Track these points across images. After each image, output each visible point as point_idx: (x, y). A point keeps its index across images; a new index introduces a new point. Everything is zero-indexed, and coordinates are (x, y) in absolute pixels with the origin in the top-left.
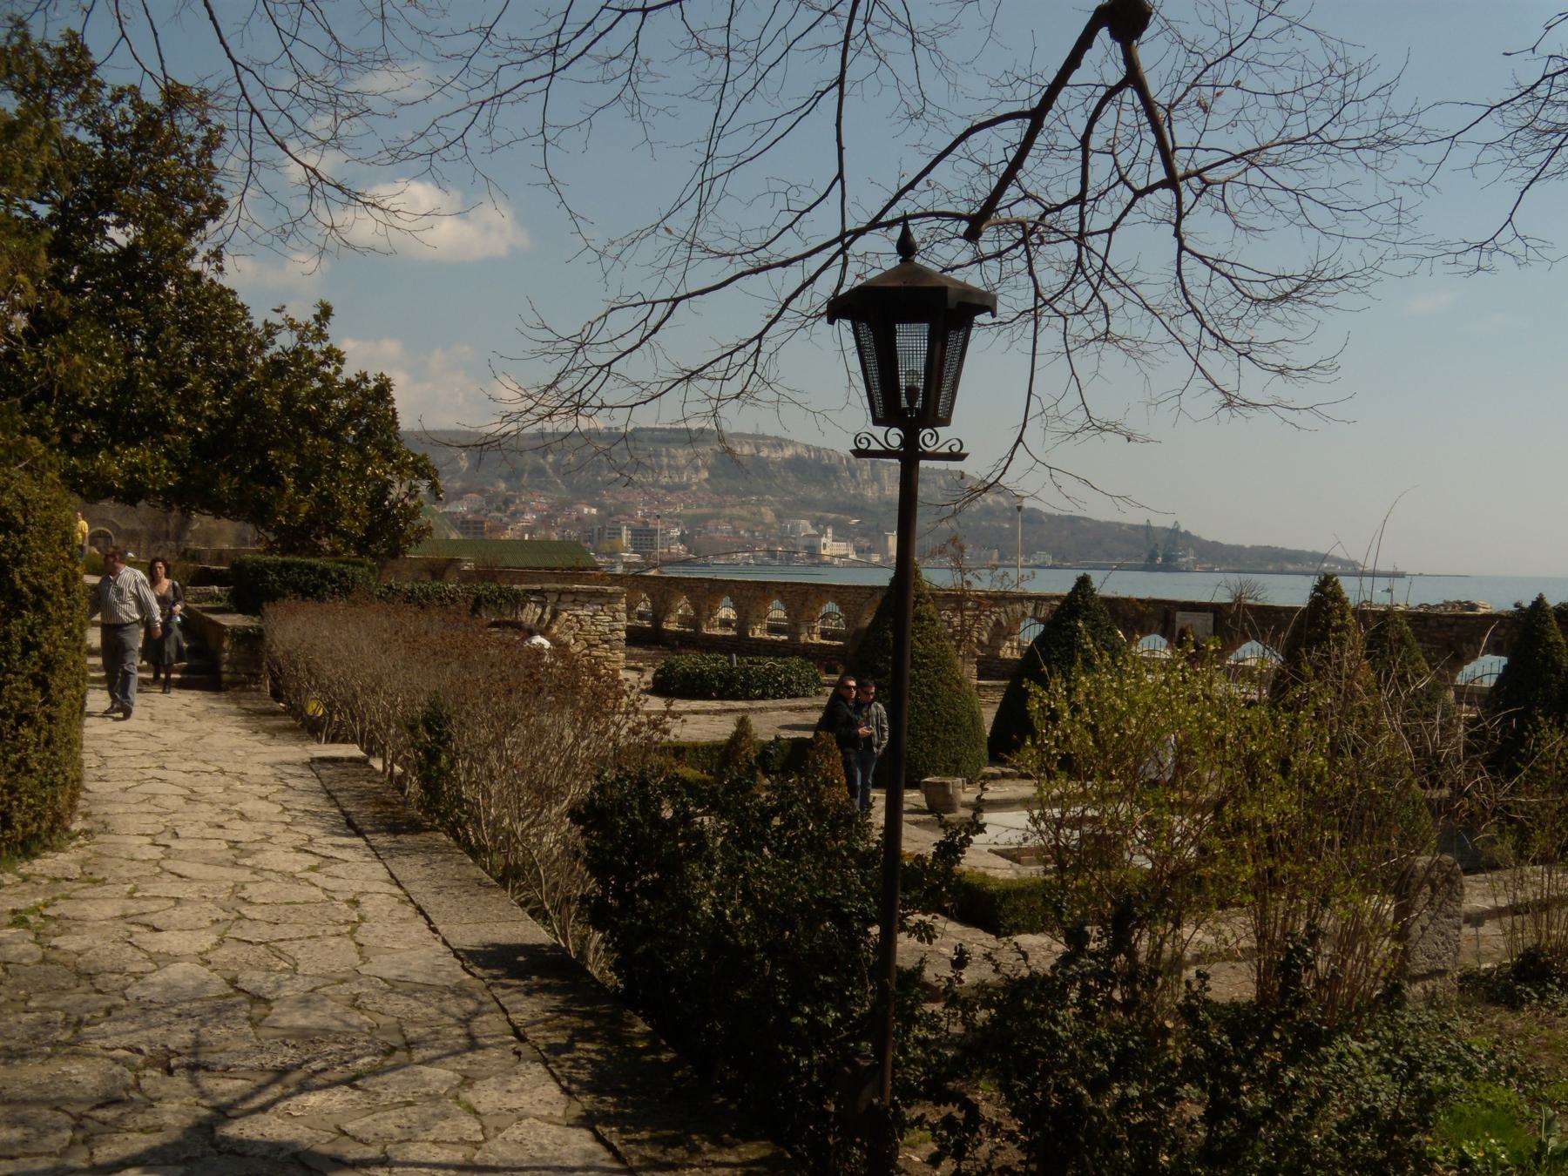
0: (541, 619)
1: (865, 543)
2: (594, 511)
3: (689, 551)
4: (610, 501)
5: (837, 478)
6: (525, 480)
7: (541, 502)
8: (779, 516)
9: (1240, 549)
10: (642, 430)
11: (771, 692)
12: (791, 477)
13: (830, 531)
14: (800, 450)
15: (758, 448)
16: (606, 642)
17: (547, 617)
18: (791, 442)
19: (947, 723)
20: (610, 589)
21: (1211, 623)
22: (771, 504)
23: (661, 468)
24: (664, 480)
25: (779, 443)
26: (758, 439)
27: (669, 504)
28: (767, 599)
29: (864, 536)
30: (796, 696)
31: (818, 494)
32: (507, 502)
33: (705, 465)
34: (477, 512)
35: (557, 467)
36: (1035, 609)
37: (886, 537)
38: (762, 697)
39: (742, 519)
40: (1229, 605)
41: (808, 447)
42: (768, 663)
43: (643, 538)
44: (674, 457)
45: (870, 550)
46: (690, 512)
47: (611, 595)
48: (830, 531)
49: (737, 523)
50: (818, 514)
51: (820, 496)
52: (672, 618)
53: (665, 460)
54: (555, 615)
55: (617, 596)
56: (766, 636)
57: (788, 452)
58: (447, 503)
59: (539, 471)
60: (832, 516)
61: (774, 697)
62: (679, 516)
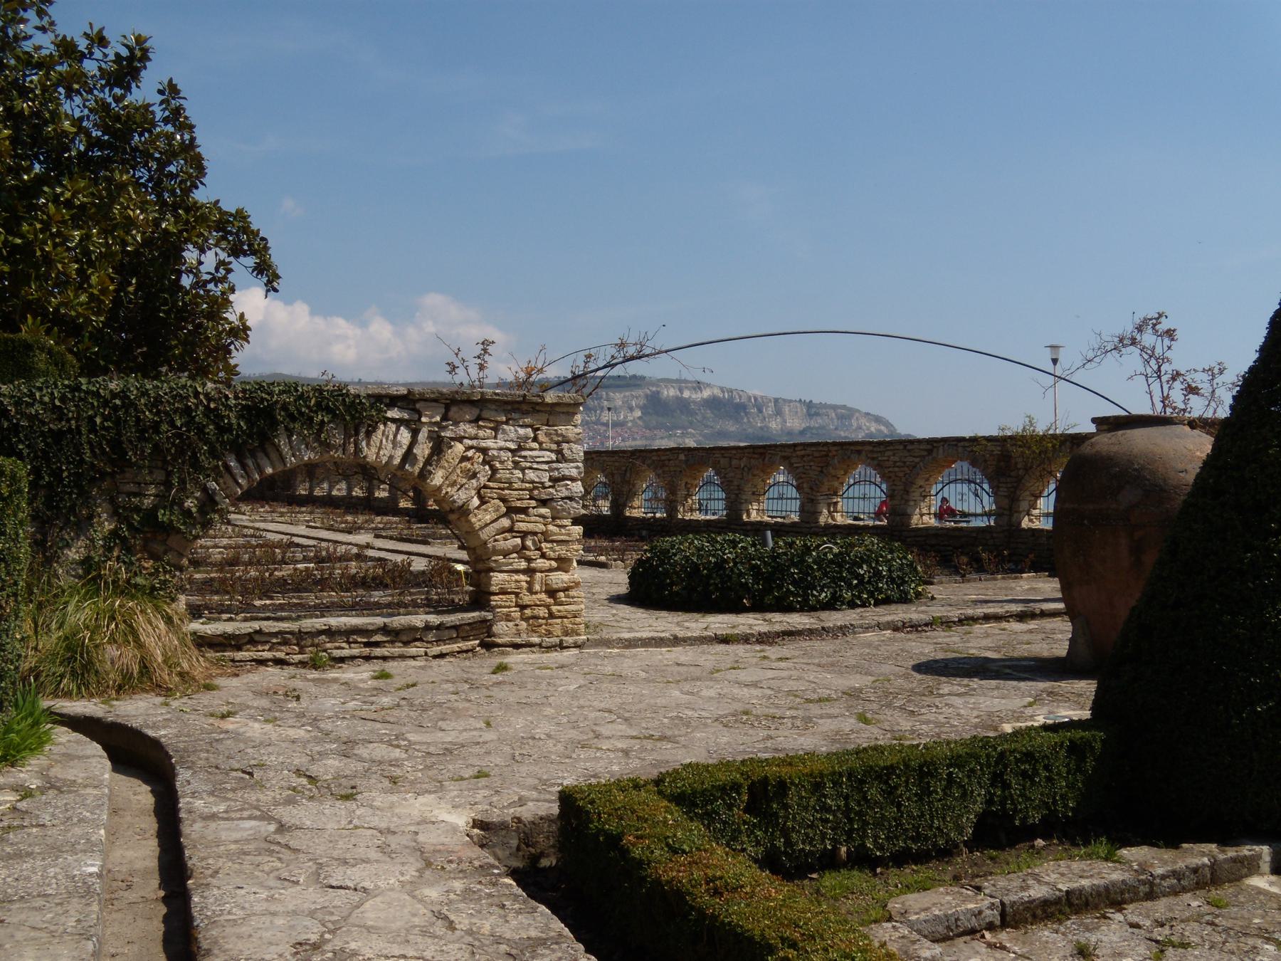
0: (409, 456)
5: (746, 414)
11: (847, 595)
12: (709, 414)
14: (717, 392)
15: (681, 390)
16: (544, 503)
17: (422, 450)
18: (708, 385)
22: (693, 436)
25: (699, 386)
26: (680, 383)
28: (768, 469)
30: (887, 601)
41: (722, 389)
51: (733, 429)
52: (636, 503)
54: (439, 446)
57: (706, 394)
61: (852, 605)
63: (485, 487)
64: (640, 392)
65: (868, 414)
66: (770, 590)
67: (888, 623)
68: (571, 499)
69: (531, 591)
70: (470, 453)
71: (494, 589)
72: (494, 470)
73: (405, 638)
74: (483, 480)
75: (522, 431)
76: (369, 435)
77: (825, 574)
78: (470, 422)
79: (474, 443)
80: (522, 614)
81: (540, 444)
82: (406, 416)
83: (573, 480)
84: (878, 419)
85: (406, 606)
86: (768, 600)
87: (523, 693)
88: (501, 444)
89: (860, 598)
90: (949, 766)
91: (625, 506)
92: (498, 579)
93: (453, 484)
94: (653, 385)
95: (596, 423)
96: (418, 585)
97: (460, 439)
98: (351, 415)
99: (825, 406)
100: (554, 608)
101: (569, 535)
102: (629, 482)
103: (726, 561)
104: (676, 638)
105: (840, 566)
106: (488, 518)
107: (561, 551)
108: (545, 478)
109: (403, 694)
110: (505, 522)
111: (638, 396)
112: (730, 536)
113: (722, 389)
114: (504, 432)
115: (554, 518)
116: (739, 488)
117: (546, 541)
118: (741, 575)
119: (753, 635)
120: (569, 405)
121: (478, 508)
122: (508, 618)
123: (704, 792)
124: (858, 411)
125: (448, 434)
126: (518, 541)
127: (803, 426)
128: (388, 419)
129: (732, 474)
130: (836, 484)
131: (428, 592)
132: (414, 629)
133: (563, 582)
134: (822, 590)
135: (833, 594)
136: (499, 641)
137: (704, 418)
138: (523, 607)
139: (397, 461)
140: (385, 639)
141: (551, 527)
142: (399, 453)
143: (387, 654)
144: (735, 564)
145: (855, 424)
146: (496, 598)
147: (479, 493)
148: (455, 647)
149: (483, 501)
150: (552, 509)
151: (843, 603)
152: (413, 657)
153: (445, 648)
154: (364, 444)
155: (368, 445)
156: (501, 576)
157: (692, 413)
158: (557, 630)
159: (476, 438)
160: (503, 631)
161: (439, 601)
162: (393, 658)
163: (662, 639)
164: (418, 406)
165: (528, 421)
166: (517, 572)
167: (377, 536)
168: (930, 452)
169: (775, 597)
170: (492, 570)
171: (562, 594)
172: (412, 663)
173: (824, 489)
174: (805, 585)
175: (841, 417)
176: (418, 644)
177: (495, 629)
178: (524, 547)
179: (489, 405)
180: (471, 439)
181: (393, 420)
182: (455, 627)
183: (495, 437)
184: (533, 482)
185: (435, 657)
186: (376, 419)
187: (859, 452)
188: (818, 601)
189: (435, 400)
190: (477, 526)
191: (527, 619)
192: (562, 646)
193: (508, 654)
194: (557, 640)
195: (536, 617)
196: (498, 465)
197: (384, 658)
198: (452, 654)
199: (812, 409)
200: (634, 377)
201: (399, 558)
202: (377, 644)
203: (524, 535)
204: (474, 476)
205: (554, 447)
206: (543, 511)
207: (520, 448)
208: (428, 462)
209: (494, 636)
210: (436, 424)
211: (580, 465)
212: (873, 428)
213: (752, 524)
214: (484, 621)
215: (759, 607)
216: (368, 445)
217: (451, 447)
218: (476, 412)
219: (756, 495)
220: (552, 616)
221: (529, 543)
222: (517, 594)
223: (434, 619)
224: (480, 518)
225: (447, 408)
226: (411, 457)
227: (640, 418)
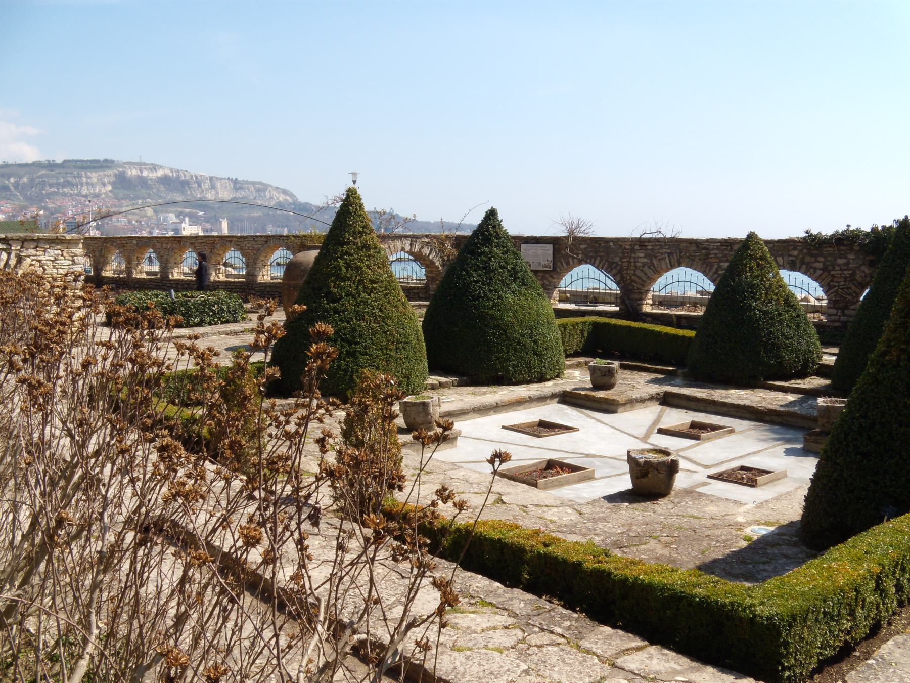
1: (208, 226)
4: (51, 206)
5: (190, 188)
8: (155, 212)
9: (428, 223)
10: (69, 161)
11: (208, 319)
12: (162, 188)
13: (187, 219)
17: (13, 262)
18: (161, 167)
19: (399, 342)
21: (551, 252)
24: (85, 191)
25: (154, 168)
28: (182, 250)
29: (207, 221)
30: (227, 322)
33: (109, 183)
35: (16, 185)
36: (411, 245)
37: (221, 222)
38: (200, 324)
40: (567, 238)
41: (171, 170)
44: (90, 178)
48: (187, 219)
50: (179, 210)
52: (108, 268)
53: (84, 180)
54: (20, 260)
57: (160, 173)
60: (187, 210)
61: (210, 324)
64: (111, 172)
65: (278, 188)
70: (34, 262)
75: (56, 252)
77: (197, 310)
84: (285, 192)
88: (47, 258)
91: (101, 270)
94: (120, 167)
95: (77, 195)
97: (29, 256)
99: (247, 182)
105: (204, 306)
111: (109, 175)
112: (155, 292)
113: (171, 170)
116: (167, 260)
124: (271, 186)
130: (219, 258)
137: (158, 191)
145: (268, 196)
157: (149, 187)
159: (36, 255)
165: (59, 247)
168: (266, 242)
173: (213, 261)
174: (187, 315)
175: (258, 190)
187: (231, 241)
199: (237, 185)
200: (106, 161)
207: (56, 259)
208: (15, 267)
212: (282, 198)
213: (174, 280)
218: (35, 244)
219: (177, 264)
225: (23, 243)
227: (110, 191)
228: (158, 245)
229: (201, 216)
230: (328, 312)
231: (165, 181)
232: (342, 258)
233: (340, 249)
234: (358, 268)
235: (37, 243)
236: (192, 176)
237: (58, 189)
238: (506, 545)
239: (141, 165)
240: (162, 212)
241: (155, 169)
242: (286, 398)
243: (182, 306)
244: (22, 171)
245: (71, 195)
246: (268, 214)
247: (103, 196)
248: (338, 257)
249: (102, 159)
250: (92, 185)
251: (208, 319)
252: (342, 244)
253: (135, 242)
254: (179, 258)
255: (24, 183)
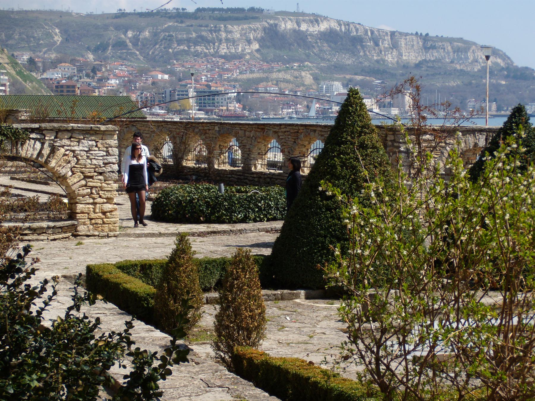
0: (40, 154)
2: (166, 77)
3: (244, 109)
4: (179, 69)
5: (363, 47)
6: (109, 51)
7: (123, 70)
8: (316, 79)
10: (204, 10)
11: (252, 216)
12: (326, 46)
14: (334, 25)
16: (101, 174)
17: (46, 151)
18: (326, 18)
20: (103, 128)
22: (310, 69)
23: (220, 41)
24: (223, 50)
25: (316, 19)
27: (228, 70)
28: (266, 139)
31: (348, 60)
32: (94, 70)
33: (255, 39)
34: (70, 78)
35: (135, 41)
38: (244, 221)
39: (287, 81)
41: (339, 23)
42: (252, 191)
43: (207, 98)
44: (231, 32)
45: (390, 105)
46: (244, 77)
47: (104, 133)
49: (282, 85)
50: (348, 77)
51: (349, 62)
52: (190, 157)
53: (224, 35)
54: (53, 150)
55: (110, 134)
56: (266, 171)
57: (323, 26)
58: (44, 71)
59: (120, 45)
60: (359, 78)
61: (255, 221)
62: (236, 80)
63: (74, 167)
64: (257, 25)
66: (214, 214)
67: (264, 229)
68: (113, 172)
69: (95, 212)
70: (67, 153)
71: (78, 211)
72: (78, 160)
73: (38, 232)
74: (73, 164)
75: (90, 143)
76: (22, 145)
77: (242, 206)
78: (67, 139)
79: (69, 148)
80: (91, 222)
81: (99, 148)
82: (39, 137)
83: (114, 164)
85: (37, 220)
86: (213, 217)
87: (87, 251)
88: (81, 148)
89: (259, 217)
90: (206, 264)
91: (182, 158)
92: (80, 207)
93: (60, 166)
94: (271, 18)
96: (43, 210)
97: (63, 146)
98: (15, 137)
99: (442, 39)
100: (105, 220)
101: (112, 188)
102: (184, 143)
103: (194, 199)
104: (160, 233)
105: (250, 202)
106: (75, 180)
107: (108, 195)
108: (101, 163)
109: (38, 251)
110: (83, 182)
113: (339, 23)
114: (83, 143)
115: (105, 180)
117: (102, 190)
118: (200, 206)
119: (196, 233)
120: (112, 131)
121: (71, 176)
122: (84, 224)
123: (126, 266)
124: (475, 44)
125: (57, 144)
126: (89, 190)
127: (419, 59)
128: (31, 138)
129: (245, 141)
130: (304, 150)
131: (49, 214)
132: (43, 228)
133: (109, 208)
134: (239, 213)
135: (245, 215)
136: (80, 233)
137: (321, 51)
138: (91, 219)
139: (35, 156)
140: (30, 232)
141: (104, 184)
142: (36, 153)
143: (30, 239)
144: (198, 200)
145: (471, 58)
146: (79, 215)
147: (71, 169)
148: (61, 236)
149: (73, 173)
150: (104, 177)
151: (250, 220)
152: (42, 240)
153: (56, 237)
154: (20, 149)
155: (22, 149)
156: (81, 206)
158: (106, 229)
159: (70, 146)
160: (82, 229)
161: (54, 218)
162: (33, 240)
163: (153, 234)
164: (44, 132)
165: (93, 138)
166: (88, 204)
167: (12, 179)
169: (216, 216)
170: (77, 203)
171: (108, 214)
172: (42, 242)
174: (230, 211)
175: (457, 50)
176: (44, 234)
177: (78, 228)
178: (92, 193)
179: (75, 132)
180: (68, 146)
181: (33, 139)
182: (61, 228)
183: (79, 146)
184: (95, 165)
185: (52, 240)
186: (25, 138)
187: (315, 131)
188: (237, 219)
189: (52, 130)
190: (71, 184)
191: (93, 224)
192: (108, 236)
193: (84, 239)
194: (106, 234)
195: (96, 224)
196: (80, 158)
197: (29, 240)
198: (59, 239)
199: (428, 42)
200: (252, 9)
201: (31, 195)
202: (26, 235)
203: (92, 188)
204: (69, 162)
205: (105, 149)
206: (101, 177)
207: (90, 150)
208: (49, 156)
209: (78, 231)
210: (52, 140)
211: (117, 157)
214: (74, 225)
215: (208, 221)
216: (22, 149)
217: (59, 150)
218: (70, 134)
220: (104, 223)
221: (94, 191)
222: (88, 214)
223: (51, 224)
224: (72, 181)
225: (57, 133)
226: (41, 155)
227: (257, 51)
228: (241, 133)
229: (376, 86)
230: (320, 209)
231: (330, 36)
232: (338, 156)
233: (338, 148)
234: (354, 168)
235: (72, 133)
236: (366, 31)
237: (189, 47)
238: (282, 369)
239: (298, 16)
240: (325, 79)
241: (317, 21)
242: (276, 289)
243: (225, 200)
244: (143, 22)
245: (206, 55)
246: (470, 84)
247: (248, 57)
248: (335, 156)
249: (246, 7)
250: (234, 42)
251: (252, 216)
252: (339, 144)
253: (217, 128)
254: (263, 148)
255: (145, 39)
